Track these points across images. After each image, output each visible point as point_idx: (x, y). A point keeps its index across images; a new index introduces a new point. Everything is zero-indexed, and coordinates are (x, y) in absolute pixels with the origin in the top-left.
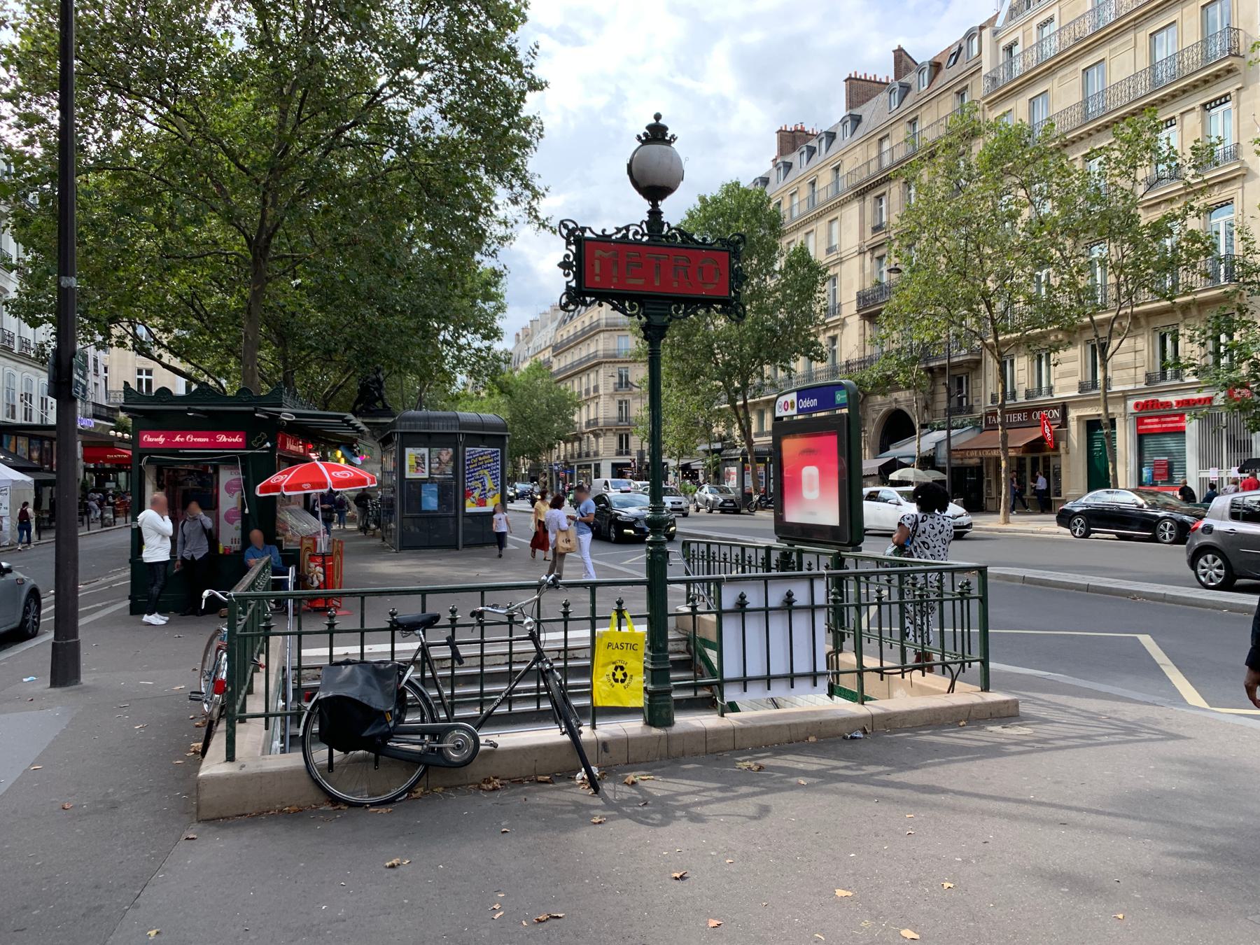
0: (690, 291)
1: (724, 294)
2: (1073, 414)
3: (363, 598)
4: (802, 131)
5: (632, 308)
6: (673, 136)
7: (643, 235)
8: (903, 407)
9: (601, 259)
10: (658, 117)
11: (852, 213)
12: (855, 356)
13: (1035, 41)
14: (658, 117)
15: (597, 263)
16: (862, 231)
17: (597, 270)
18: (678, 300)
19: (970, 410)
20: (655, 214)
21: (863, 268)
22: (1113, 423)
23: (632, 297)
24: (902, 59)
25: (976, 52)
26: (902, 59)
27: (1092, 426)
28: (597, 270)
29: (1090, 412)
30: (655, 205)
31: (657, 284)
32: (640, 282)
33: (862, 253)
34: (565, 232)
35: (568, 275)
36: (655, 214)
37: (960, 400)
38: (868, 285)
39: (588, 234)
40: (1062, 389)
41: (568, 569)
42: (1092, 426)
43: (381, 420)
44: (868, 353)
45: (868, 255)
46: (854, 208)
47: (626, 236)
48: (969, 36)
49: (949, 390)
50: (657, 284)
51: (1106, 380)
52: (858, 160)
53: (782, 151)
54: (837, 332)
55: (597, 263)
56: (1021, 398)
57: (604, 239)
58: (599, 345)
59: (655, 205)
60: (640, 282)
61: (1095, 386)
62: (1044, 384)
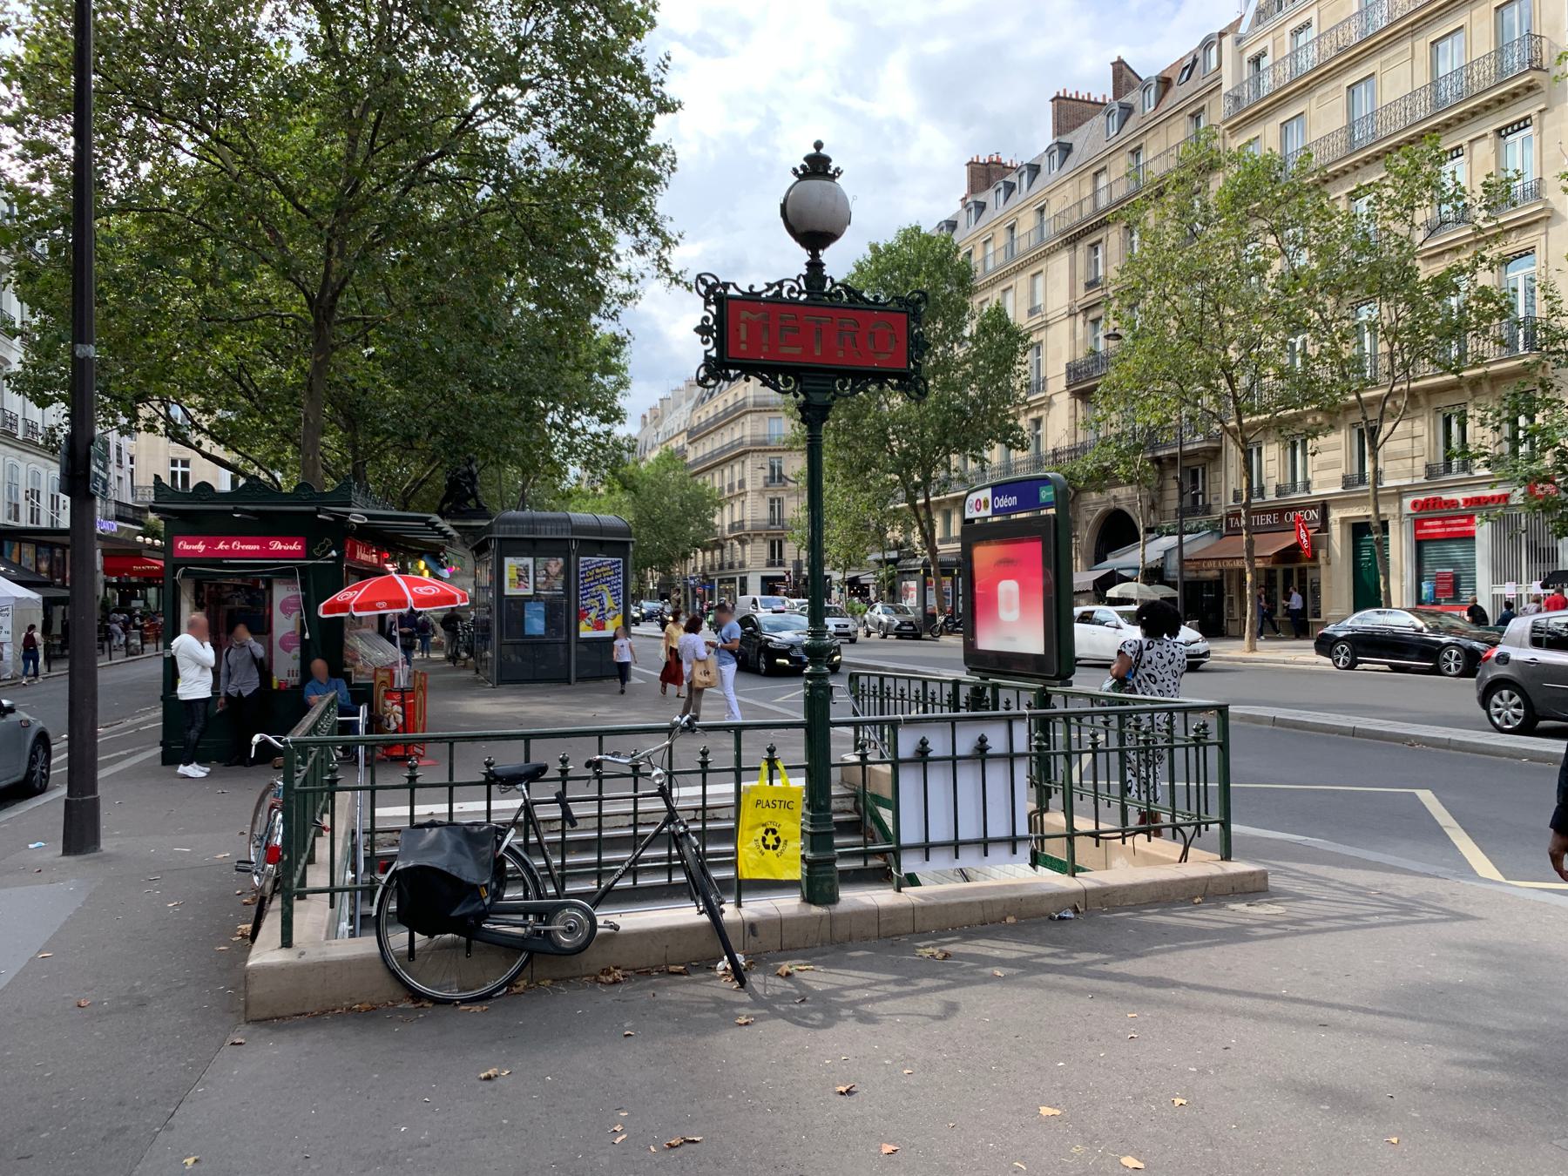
0: (858, 362)
1: (900, 366)
2: (1335, 515)
3: (451, 744)
4: (998, 163)
5: (787, 383)
6: (837, 169)
7: (800, 293)
8: (1124, 507)
9: (748, 322)
10: (818, 145)
11: (1060, 265)
12: (1064, 443)
13: (1287, 52)
14: (818, 145)
15: (743, 328)
16: (1073, 287)
17: (743, 336)
18: (844, 374)
19: (1207, 510)
20: (815, 266)
21: (1074, 333)
22: (1384, 526)
23: (786, 370)
24: (1122, 74)
25: (1214, 65)
26: (1122, 74)
27: (1359, 530)
28: (743, 336)
29: (1357, 512)
30: (815, 256)
31: (818, 353)
32: (797, 351)
33: (1072, 315)
34: (703, 288)
35: (706, 342)
36: (815, 266)
37: (1195, 498)
38: (1080, 355)
39: (732, 291)
40: (1322, 484)
41: (707, 708)
42: (1359, 530)
43: (474, 523)
44: (1080, 439)
45: (1080, 318)
46: (1063, 259)
47: (779, 294)
48: (1206, 45)
49: (1181, 486)
50: (818, 353)
51: (1377, 473)
52: (1067, 199)
53: (974, 188)
54: (1042, 413)
55: (743, 328)
56: (1271, 495)
57: (751, 297)
58: (746, 430)
59: (815, 256)
60: (797, 351)
61: (1362, 480)
62: (1299, 478)
